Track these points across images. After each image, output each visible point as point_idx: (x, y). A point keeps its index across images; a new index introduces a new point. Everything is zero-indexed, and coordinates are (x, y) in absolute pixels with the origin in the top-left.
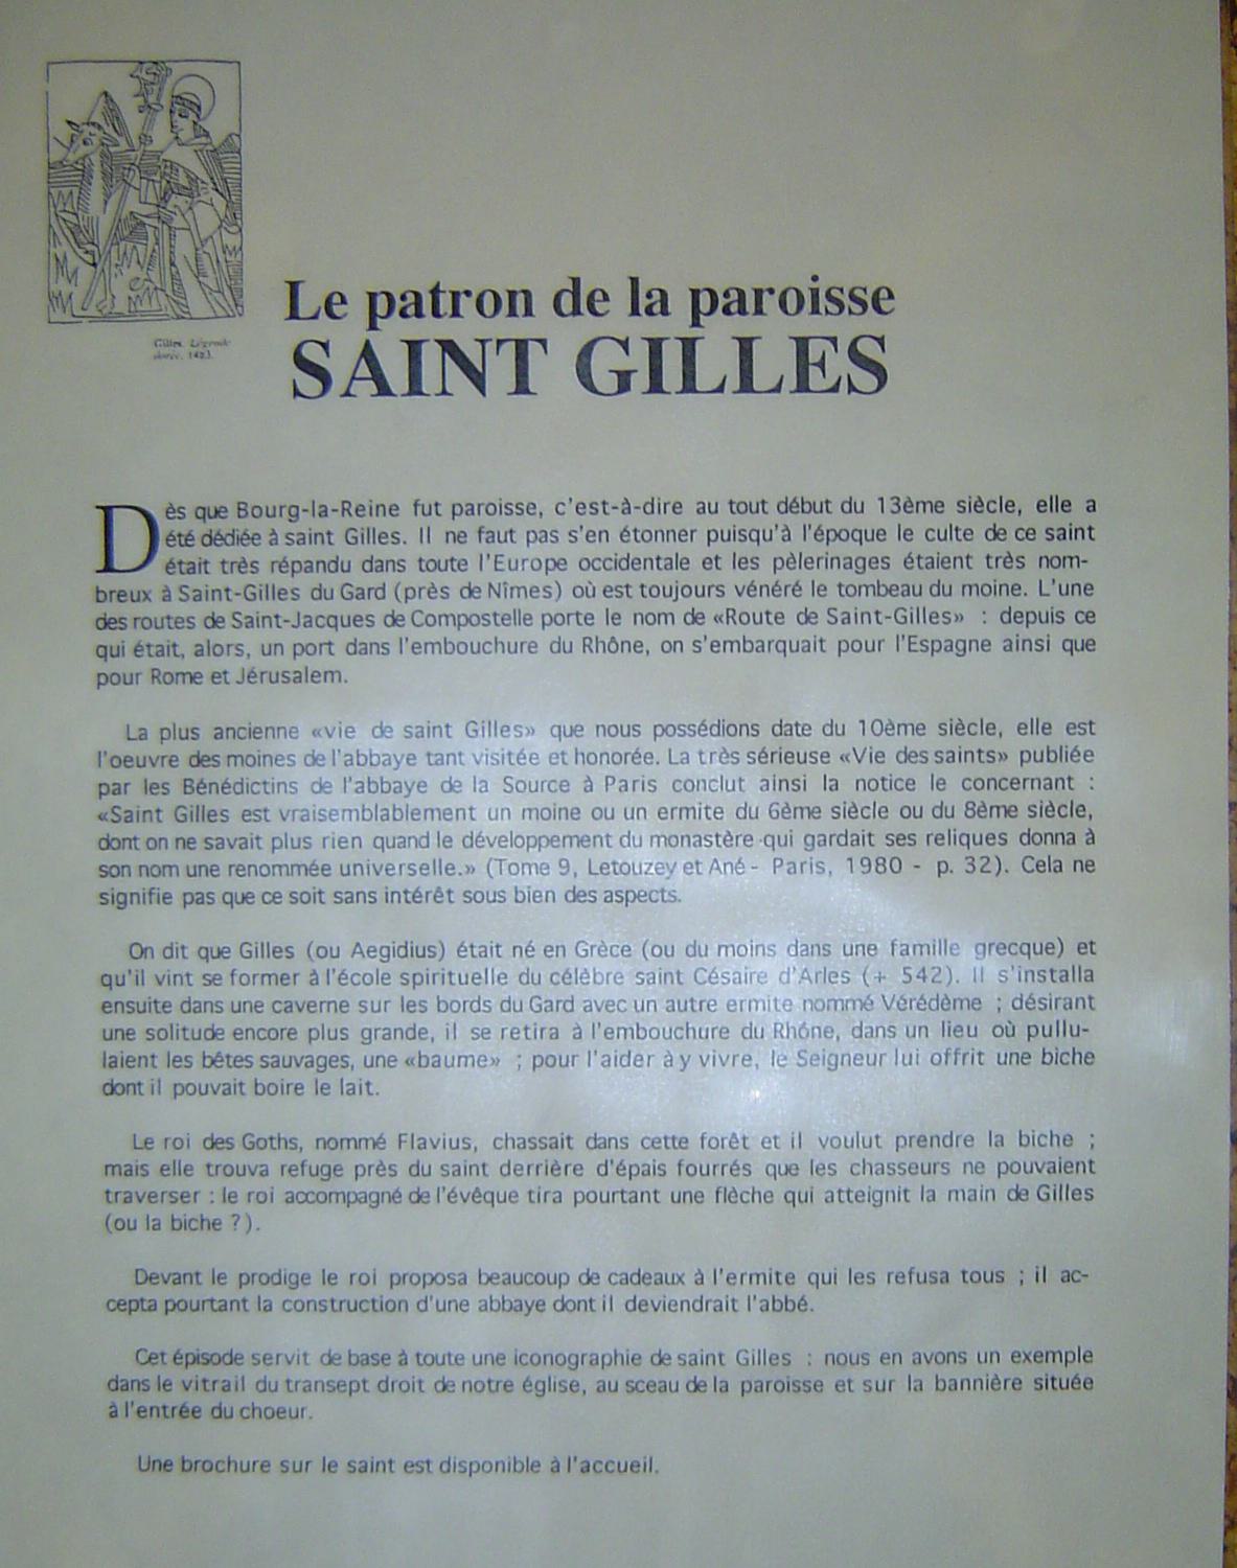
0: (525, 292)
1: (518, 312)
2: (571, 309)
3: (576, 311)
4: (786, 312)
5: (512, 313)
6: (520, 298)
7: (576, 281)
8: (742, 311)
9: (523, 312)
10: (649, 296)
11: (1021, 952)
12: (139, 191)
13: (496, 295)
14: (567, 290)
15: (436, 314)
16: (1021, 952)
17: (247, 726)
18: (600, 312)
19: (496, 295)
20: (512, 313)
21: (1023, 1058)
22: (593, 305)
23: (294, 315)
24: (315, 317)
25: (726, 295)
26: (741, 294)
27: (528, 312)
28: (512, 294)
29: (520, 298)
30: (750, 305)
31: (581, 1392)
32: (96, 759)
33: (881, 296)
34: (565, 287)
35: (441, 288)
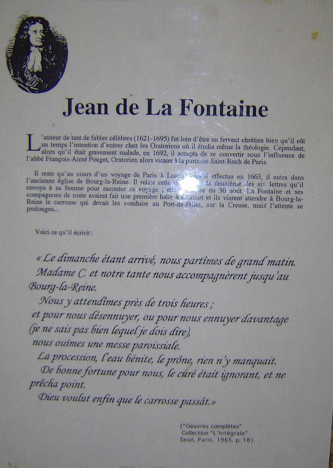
0: (213, 105)
1: (102, 112)
2: (123, 112)
3: (125, 113)
4: (197, 114)
5: (208, 114)
6: (103, 107)
7: (125, 100)
8: (93, 113)
9: (104, 113)
10: (229, 108)
11: (128, 205)
12: (41, 59)
13: (202, 106)
14: (122, 104)
15: (222, 114)
16: (128, 205)
17: (40, 179)
18: (264, 115)
19: (202, 106)
20: (208, 114)
21: (213, 205)
22: (132, 110)
23: (150, 113)
24: (158, 114)
25: (87, 106)
26: (93, 106)
27: (106, 113)
28: (208, 107)
29: (103, 107)
30: (96, 110)
31: (247, 207)
32: (26, 180)
33: (262, 109)
34: (122, 103)
35: (224, 104)
